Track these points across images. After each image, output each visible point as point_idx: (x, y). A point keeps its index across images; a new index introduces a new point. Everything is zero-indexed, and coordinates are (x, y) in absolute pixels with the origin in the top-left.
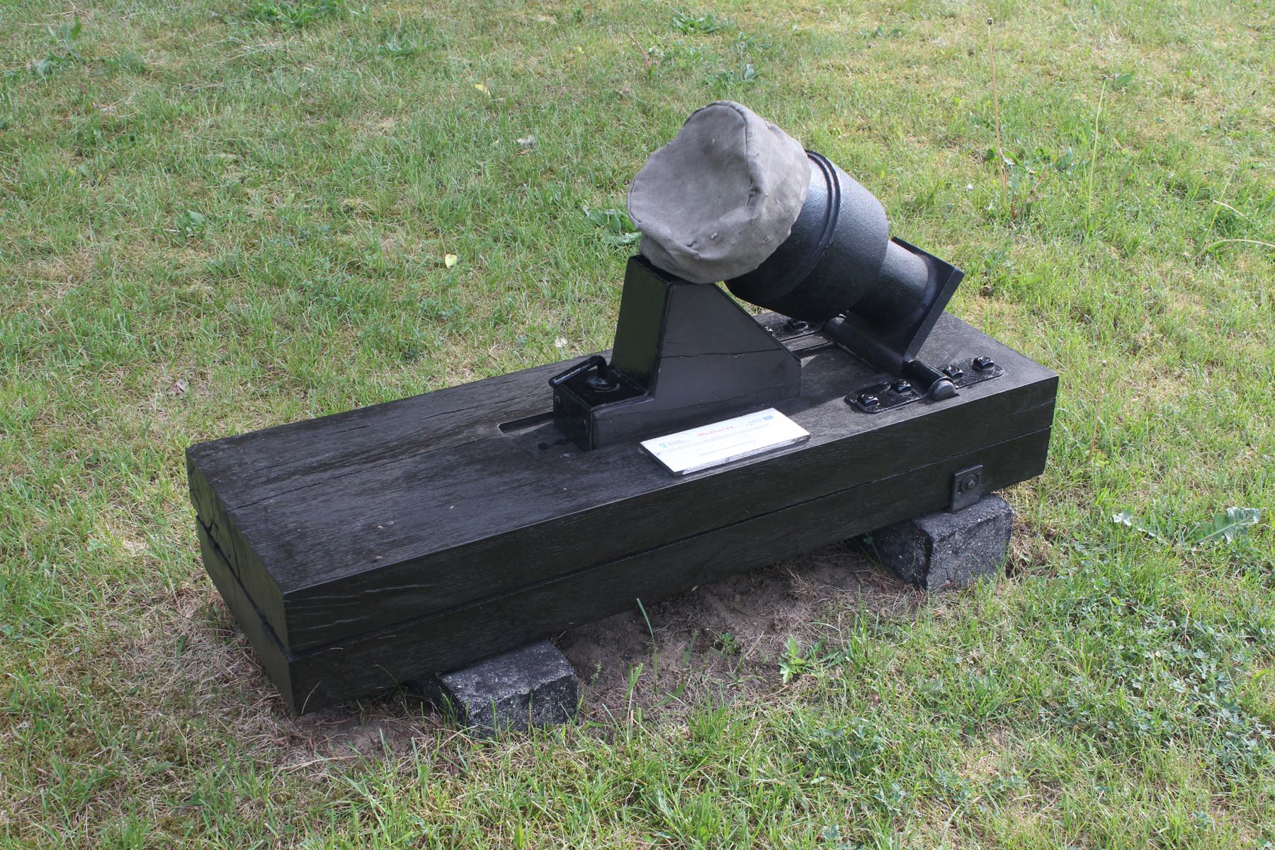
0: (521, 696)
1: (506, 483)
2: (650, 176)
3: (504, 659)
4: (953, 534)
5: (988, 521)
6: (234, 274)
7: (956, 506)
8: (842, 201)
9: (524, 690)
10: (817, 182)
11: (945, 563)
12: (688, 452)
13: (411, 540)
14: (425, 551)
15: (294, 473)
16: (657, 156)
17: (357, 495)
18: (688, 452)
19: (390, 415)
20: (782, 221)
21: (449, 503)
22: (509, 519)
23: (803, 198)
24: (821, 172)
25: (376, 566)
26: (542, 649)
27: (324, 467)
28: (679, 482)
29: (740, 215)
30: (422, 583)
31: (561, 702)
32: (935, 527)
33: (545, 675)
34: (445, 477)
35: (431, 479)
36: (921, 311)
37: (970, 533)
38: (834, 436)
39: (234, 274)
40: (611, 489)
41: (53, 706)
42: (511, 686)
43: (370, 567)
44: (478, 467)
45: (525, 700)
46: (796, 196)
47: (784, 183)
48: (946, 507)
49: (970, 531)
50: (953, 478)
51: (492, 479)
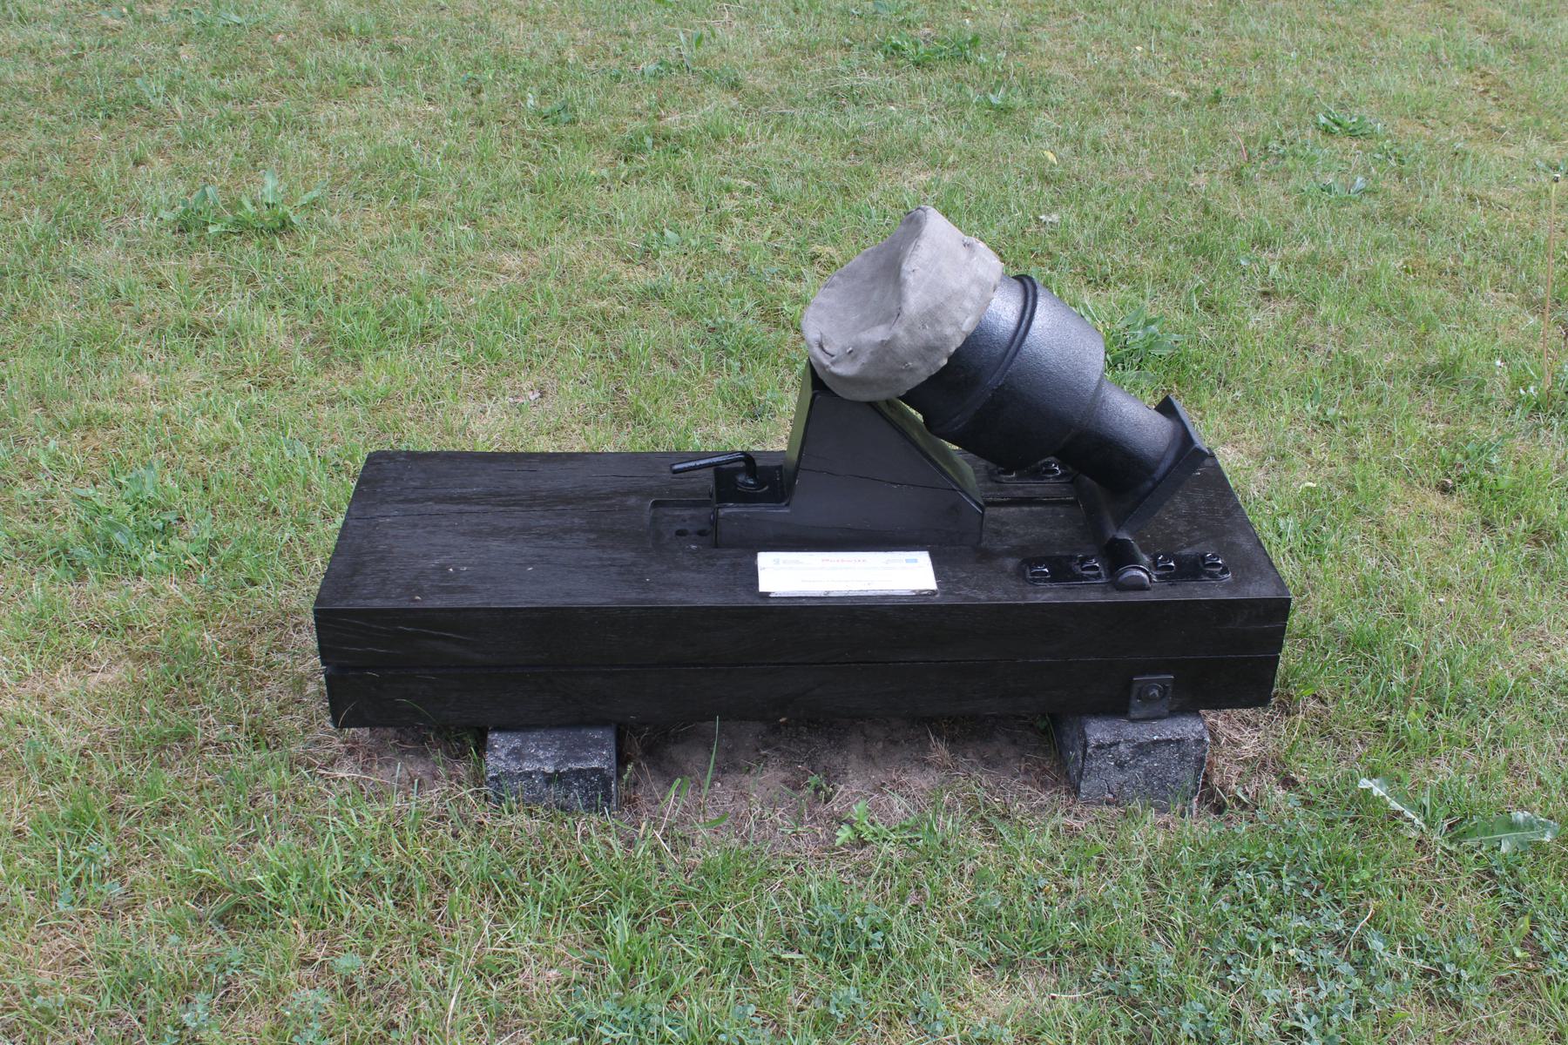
0: (544, 773)
1: (600, 559)
2: (853, 274)
3: (557, 734)
4: (1117, 744)
5: (1169, 742)
6: (661, 296)
7: (1134, 714)
8: (1028, 340)
9: (549, 769)
10: (1005, 309)
11: (1101, 776)
12: (785, 574)
13: (464, 589)
14: (466, 604)
15: (430, 499)
16: (867, 255)
17: (463, 534)
18: (785, 574)
19: (569, 465)
20: (931, 349)
21: (531, 564)
22: (568, 594)
23: (968, 325)
24: (1020, 306)
25: (412, 605)
26: (597, 735)
27: (464, 499)
28: (761, 603)
29: (879, 334)
30: (552, 645)
31: (598, 792)
32: (1098, 731)
33: (578, 759)
34: (555, 538)
35: (540, 536)
36: (1150, 484)
37: (1142, 749)
38: (967, 598)
39: (661, 296)
40: (692, 587)
41: (1264, 765)
42: (540, 761)
43: (405, 605)
44: (593, 536)
45: (549, 779)
46: (957, 324)
47: (940, 307)
48: (1116, 708)
49: (1140, 746)
50: (1129, 684)
51: (594, 551)
